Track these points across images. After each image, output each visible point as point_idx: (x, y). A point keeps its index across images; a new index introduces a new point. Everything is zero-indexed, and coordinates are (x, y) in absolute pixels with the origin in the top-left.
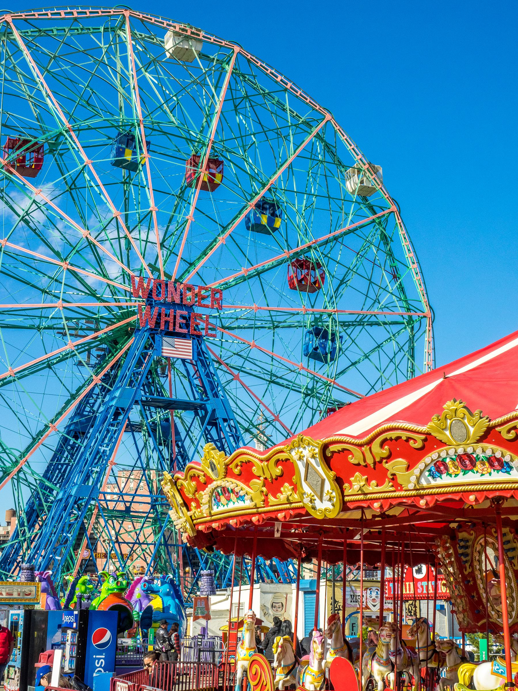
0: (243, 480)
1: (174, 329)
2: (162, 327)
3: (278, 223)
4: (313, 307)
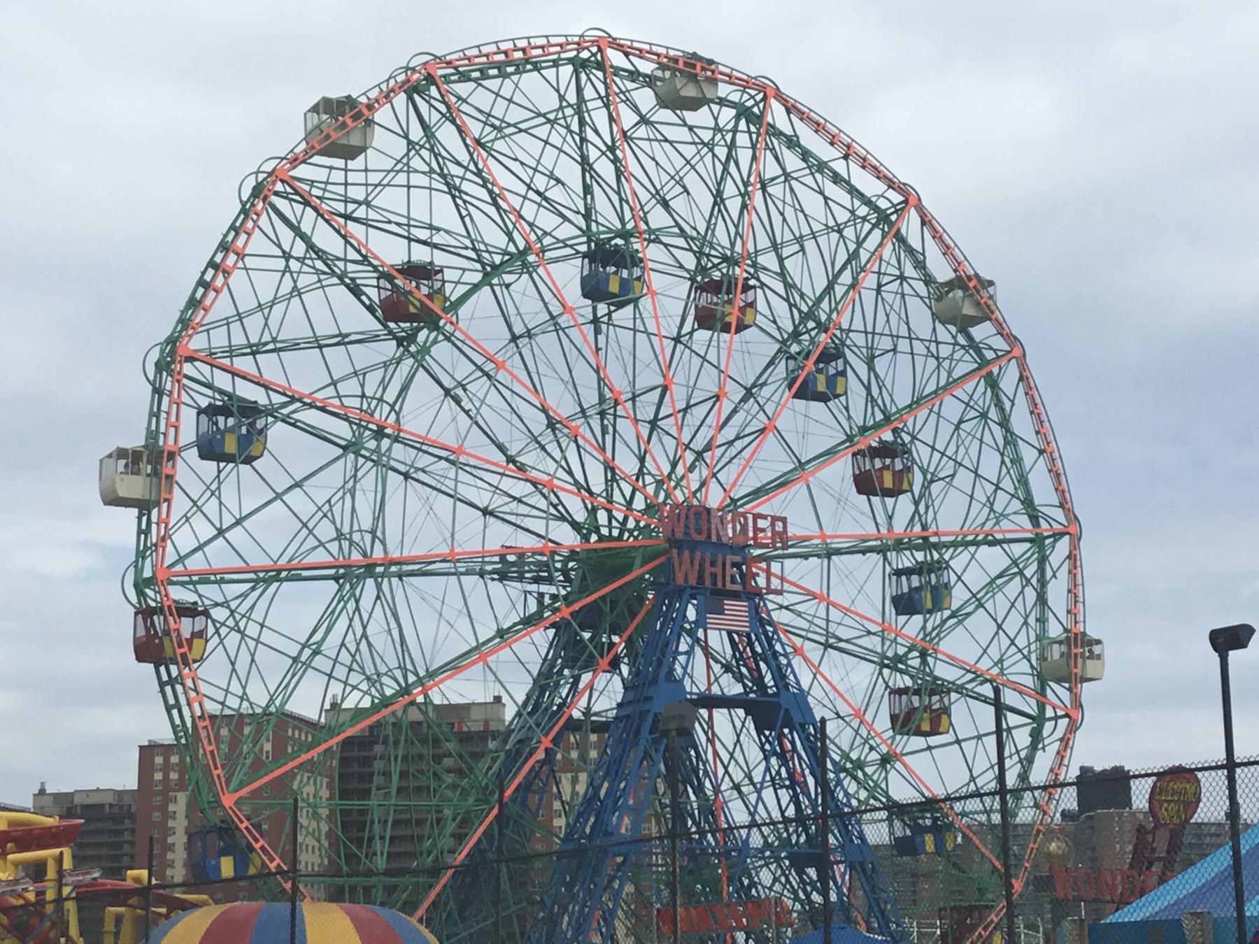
1: (724, 585)
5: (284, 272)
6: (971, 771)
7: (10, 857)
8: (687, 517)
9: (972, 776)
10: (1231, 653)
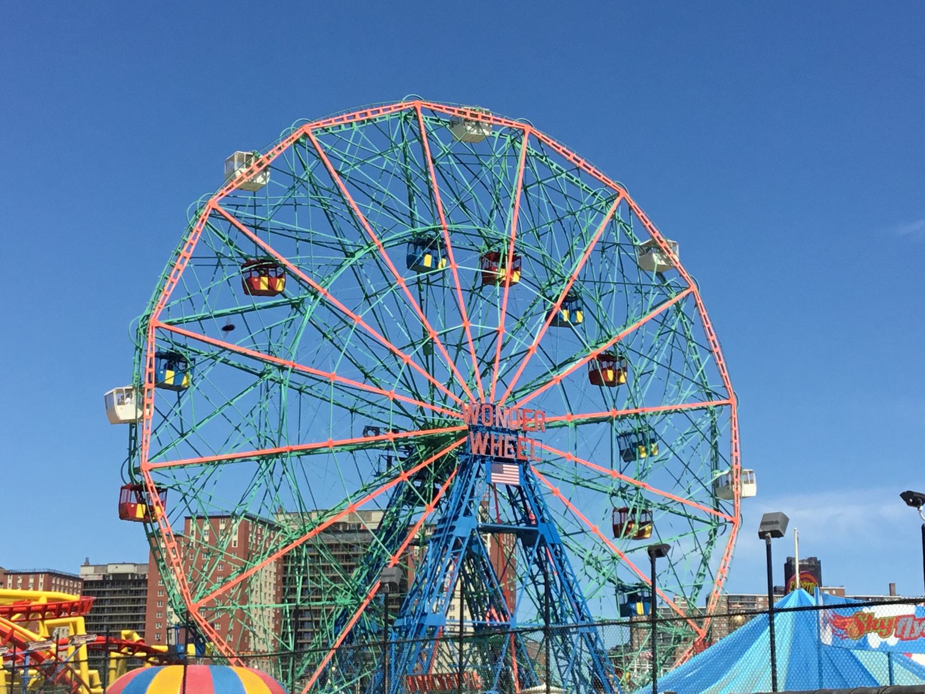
0: (904, 692)
1: (503, 455)
2: (493, 454)
3: (622, 379)
4: (621, 473)
5: (217, 266)
6: (670, 561)
7: (46, 622)
8: (480, 411)
9: (671, 564)
10: (657, 559)
